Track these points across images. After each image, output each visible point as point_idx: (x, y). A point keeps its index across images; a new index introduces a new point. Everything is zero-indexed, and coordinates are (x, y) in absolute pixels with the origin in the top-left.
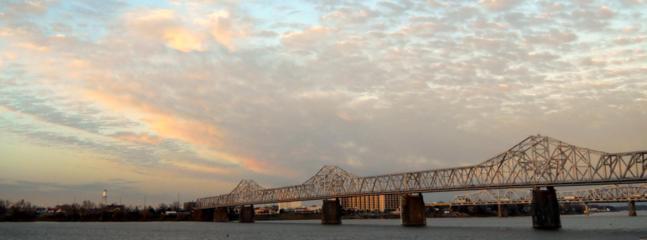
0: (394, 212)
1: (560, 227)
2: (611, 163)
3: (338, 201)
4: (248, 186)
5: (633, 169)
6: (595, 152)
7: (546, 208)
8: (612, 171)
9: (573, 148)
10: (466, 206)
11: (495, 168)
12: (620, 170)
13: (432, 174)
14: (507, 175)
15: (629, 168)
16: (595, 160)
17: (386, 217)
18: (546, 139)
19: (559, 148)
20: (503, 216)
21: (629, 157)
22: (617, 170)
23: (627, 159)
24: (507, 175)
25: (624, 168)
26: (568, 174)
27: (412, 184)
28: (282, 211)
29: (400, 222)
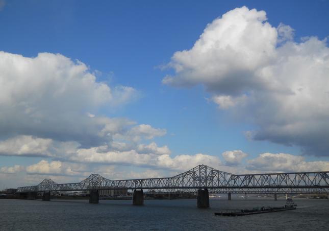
0: (119, 197)
1: (210, 206)
2: (249, 178)
3: (49, 193)
4: (48, 183)
5: (245, 182)
6: (228, 174)
7: (203, 195)
8: (235, 182)
9: (218, 171)
10: (153, 195)
11: (181, 179)
12: (239, 182)
13: (125, 182)
14: (186, 182)
15: (243, 182)
16: (228, 177)
17: (114, 199)
18: (206, 167)
19: (212, 171)
20: (171, 199)
21: (244, 177)
22: (237, 181)
23: (242, 178)
24: (186, 182)
25: (241, 182)
26: (215, 183)
27: (139, 184)
28: (62, 195)
29: (131, 202)
